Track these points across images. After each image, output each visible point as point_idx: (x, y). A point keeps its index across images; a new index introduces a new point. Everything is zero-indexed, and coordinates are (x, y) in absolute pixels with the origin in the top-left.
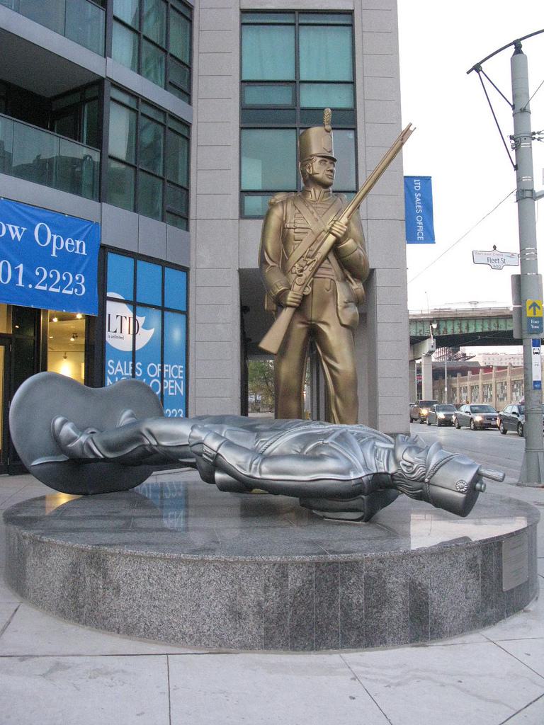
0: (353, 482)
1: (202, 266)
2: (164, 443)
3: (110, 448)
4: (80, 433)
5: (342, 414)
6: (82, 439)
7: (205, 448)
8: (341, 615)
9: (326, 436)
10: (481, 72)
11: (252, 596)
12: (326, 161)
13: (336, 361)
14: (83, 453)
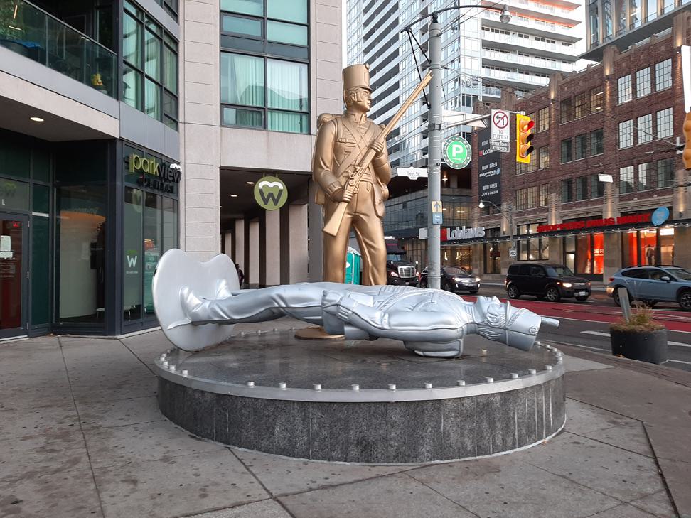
1: (189, 162)
10: (410, 34)
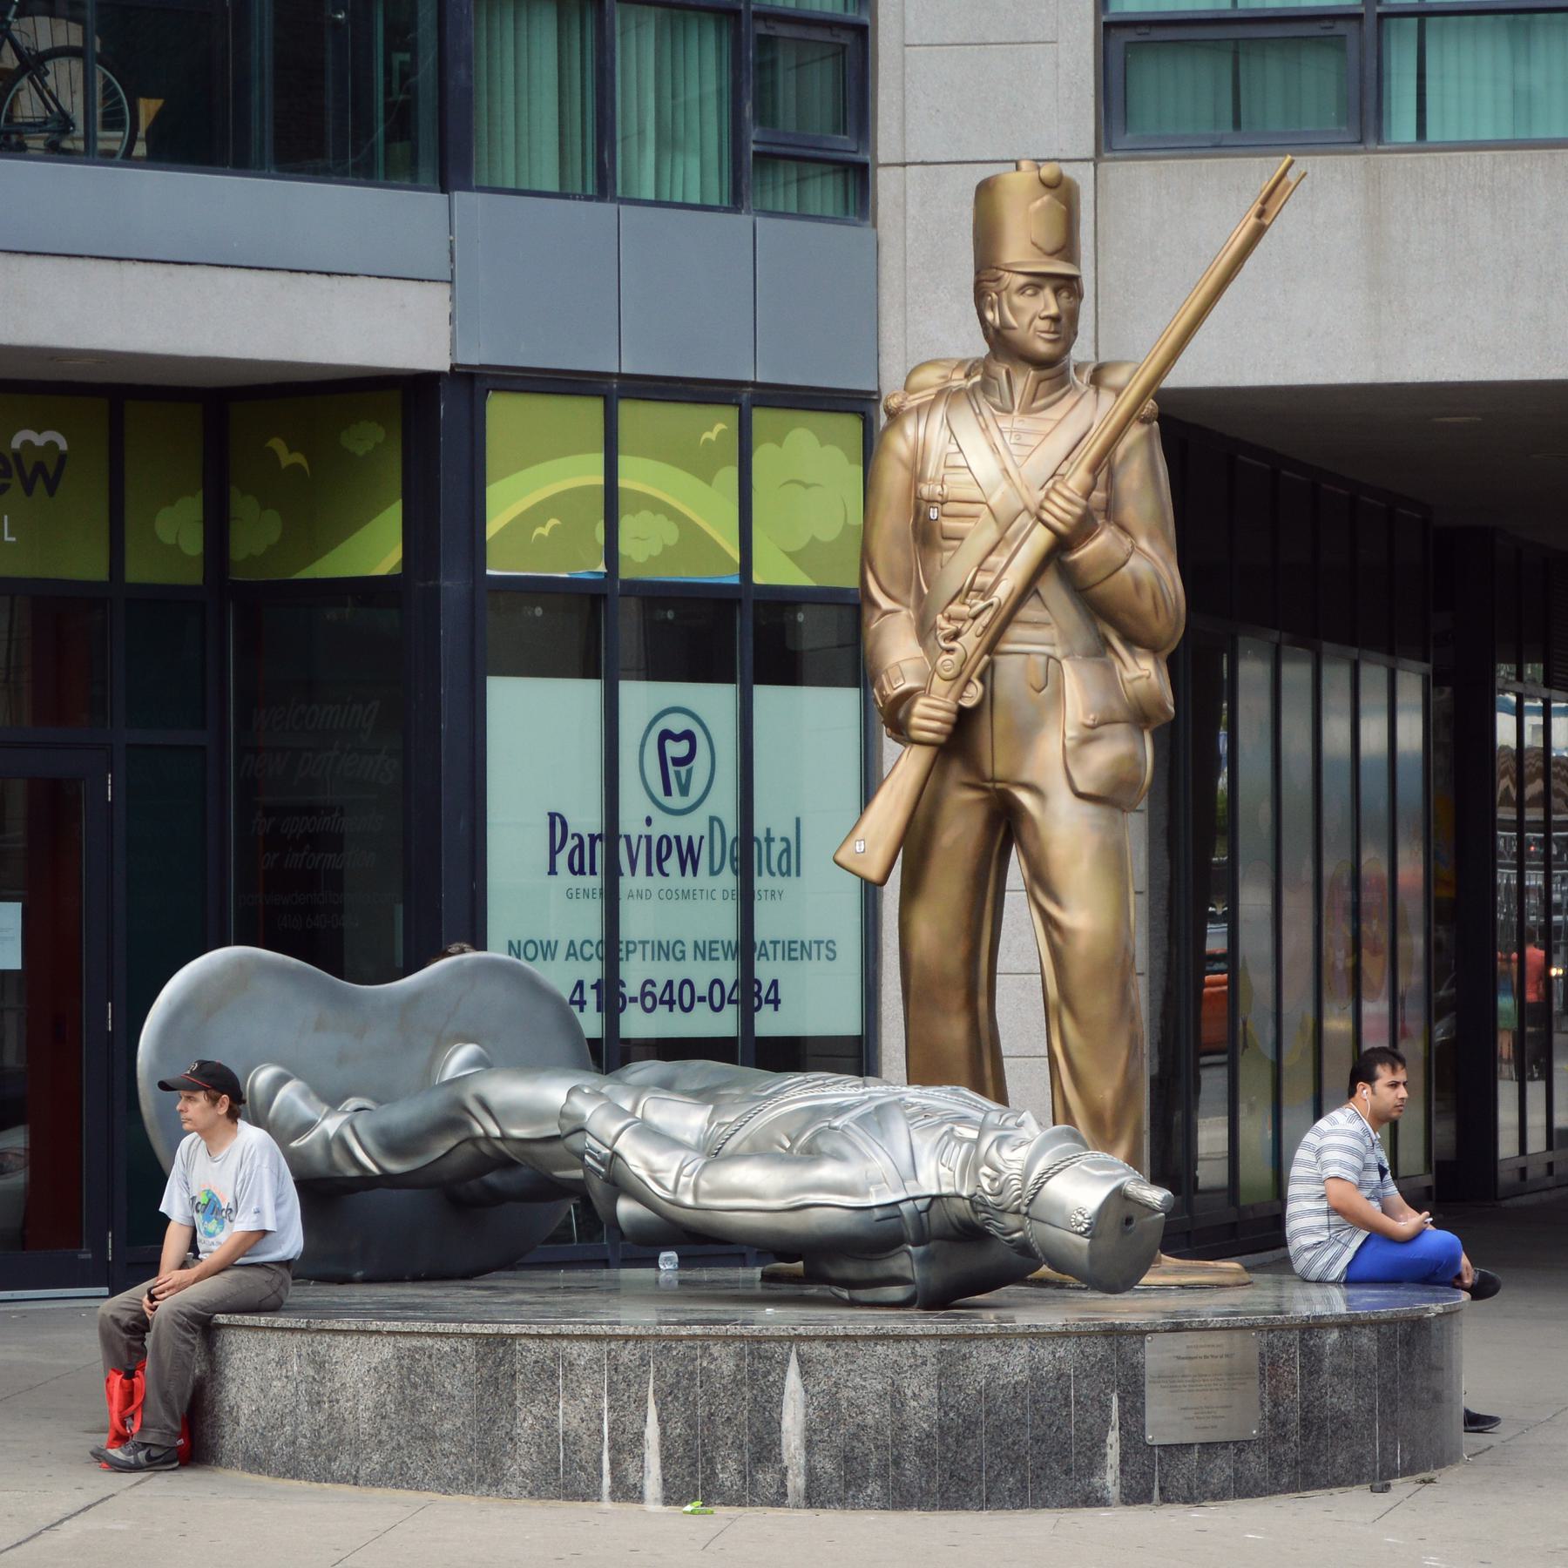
0: (877, 1213)
2: (516, 1132)
3: (394, 1145)
4: (326, 1108)
5: (1080, 1060)
6: (331, 1125)
7: (590, 1140)
8: (751, 1441)
9: (840, 1110)
11: (586, 1400)
13: (1057, 901)
14: (332, 1165)
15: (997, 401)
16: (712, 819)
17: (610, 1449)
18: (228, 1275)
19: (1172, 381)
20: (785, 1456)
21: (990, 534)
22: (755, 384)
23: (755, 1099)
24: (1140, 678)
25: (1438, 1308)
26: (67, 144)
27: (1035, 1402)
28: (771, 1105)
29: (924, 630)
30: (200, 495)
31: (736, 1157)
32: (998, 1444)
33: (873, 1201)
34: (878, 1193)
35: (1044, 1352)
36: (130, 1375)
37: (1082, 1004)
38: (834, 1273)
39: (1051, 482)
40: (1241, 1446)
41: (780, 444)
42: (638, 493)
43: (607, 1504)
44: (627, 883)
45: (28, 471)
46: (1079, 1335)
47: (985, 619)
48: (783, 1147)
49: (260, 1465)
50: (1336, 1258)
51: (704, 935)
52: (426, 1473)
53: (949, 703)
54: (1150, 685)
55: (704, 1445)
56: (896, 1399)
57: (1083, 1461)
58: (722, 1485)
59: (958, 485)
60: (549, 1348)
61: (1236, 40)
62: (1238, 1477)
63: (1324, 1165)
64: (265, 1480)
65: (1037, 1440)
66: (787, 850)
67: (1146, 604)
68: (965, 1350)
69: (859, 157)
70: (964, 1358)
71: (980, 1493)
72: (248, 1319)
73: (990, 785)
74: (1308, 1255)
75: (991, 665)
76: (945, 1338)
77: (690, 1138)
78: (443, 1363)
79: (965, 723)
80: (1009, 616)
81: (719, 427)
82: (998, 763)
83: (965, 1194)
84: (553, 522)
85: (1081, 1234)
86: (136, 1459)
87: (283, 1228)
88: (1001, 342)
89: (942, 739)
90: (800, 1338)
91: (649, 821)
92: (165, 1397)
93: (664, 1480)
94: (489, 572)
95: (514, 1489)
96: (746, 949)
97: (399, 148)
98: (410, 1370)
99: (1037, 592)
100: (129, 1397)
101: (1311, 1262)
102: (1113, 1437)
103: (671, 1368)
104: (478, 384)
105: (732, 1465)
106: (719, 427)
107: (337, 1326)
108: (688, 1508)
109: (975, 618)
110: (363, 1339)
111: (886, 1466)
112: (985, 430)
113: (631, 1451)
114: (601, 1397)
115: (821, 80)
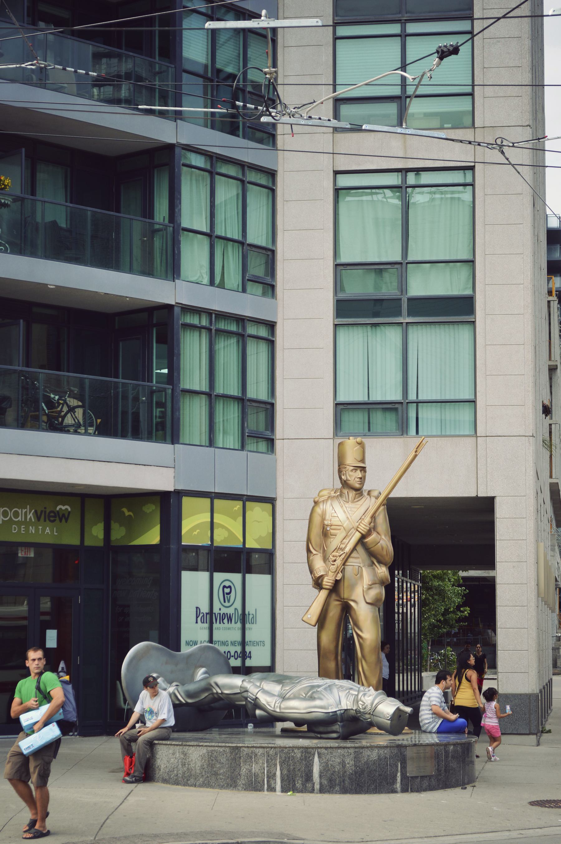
0: (331, 714)
3: (189, 695)
4: (169, 685)
5: (367, 673)
7: (249, 694)
9: (319, 686)
12: (356, 470)
13: (361, 631)
15: (345, 499)
16: (236, 609)
17: (267, 777)
18: (157, 730)
19: (392, 495)
20: (314, 780)
21: (344, 534)
22: (247, 495)
23: (294, 683)
24: (382, 572)
25: (474, 740)
26: (79, 431)
27: (379, 765)
28: (299, 685)
29: (325, 559)
30: (103, 523)
31: (289, 699)
32: (369, 777)
33: (330, 711)
34: (331, 708)
35: (381, 752)
36: (131, 757)
37: (368, 658)
38: (316, 730)
39: (360, 521)
40: (430, 777)
41: (253, 511)
42: (219, 523)
43: (266, 792)
44: (215, 626)
45: (61, 515)
46: (390, 747)
47: (343, 556)
48: (303, 696)
49: (167, 782)
50: (435, 726)
51: (234, 639)
52: (215, 784)
53: (333, 578)
54: (385, 574)
55: (292, 776)
56: (343, 764)
57: (391, 781)
58: (297, 787)
59: (335, 521)
60: (250, 750)
61: (369, 409)
62: (429, 785)
63: (431, 702)
64: (168, 786)
65: (380, 775)
66: (253, 617)
67: (385, 553)
68: (361, 751)
69: (272, 437)
70: (361, 753)
71: (365, 789)
72: (164, 742)
73: (343, 600)
74: (427, 725)
75: (344, 568)
76: (356, 748)
77: (276, 693)
78: (220, 754)
79: (337, 583)
80: (349, 556)
81: (238, 506)
82: (345, 594)
83: (354, 709)
84: (198, 531)
85: (388, 720)
86: (132, 780)
87: (169, 718)
88: (345, 484)
89: (331, 588)
90: (318, 748)
91: (220, 609)
92: (140, 763)
93: (282, 786)
94: (182, 544)
95: (240, 788)
96: (243, 643)
97: (160, 432)
98: (211, 756)
99: (356, 549)
100: (131, 763)
101: (428, 727)
102: (399, 774)
103: (283, 756)
104: (180, 494)
105: (300, 782)
106: (238, 506)
107: (191, 744)
108: (289, 794)
109: (340, 556)
110: (198, 747)
111: (341, 782)
112: (342, 507)
113: (272, 778)
114: (264, 763)
115: (262, 416)
